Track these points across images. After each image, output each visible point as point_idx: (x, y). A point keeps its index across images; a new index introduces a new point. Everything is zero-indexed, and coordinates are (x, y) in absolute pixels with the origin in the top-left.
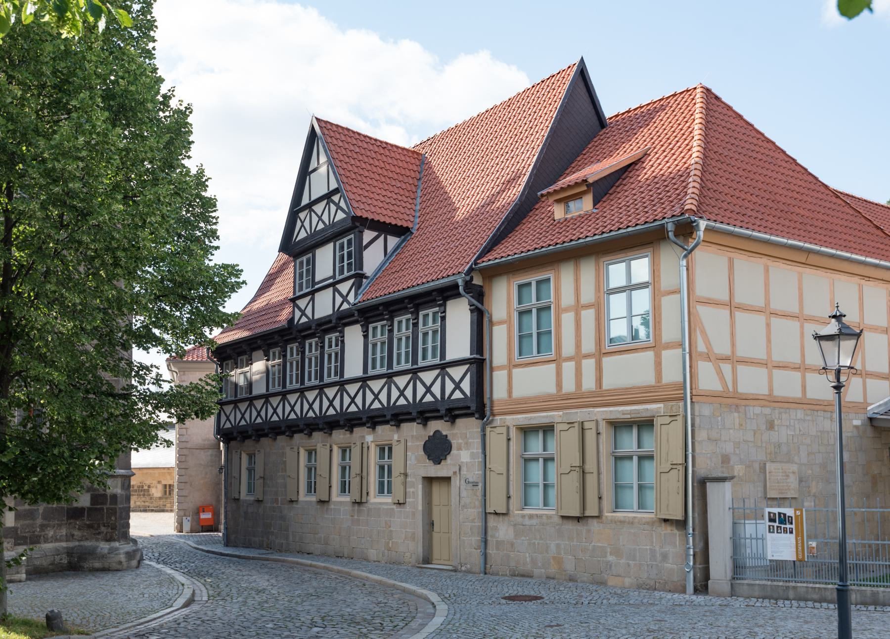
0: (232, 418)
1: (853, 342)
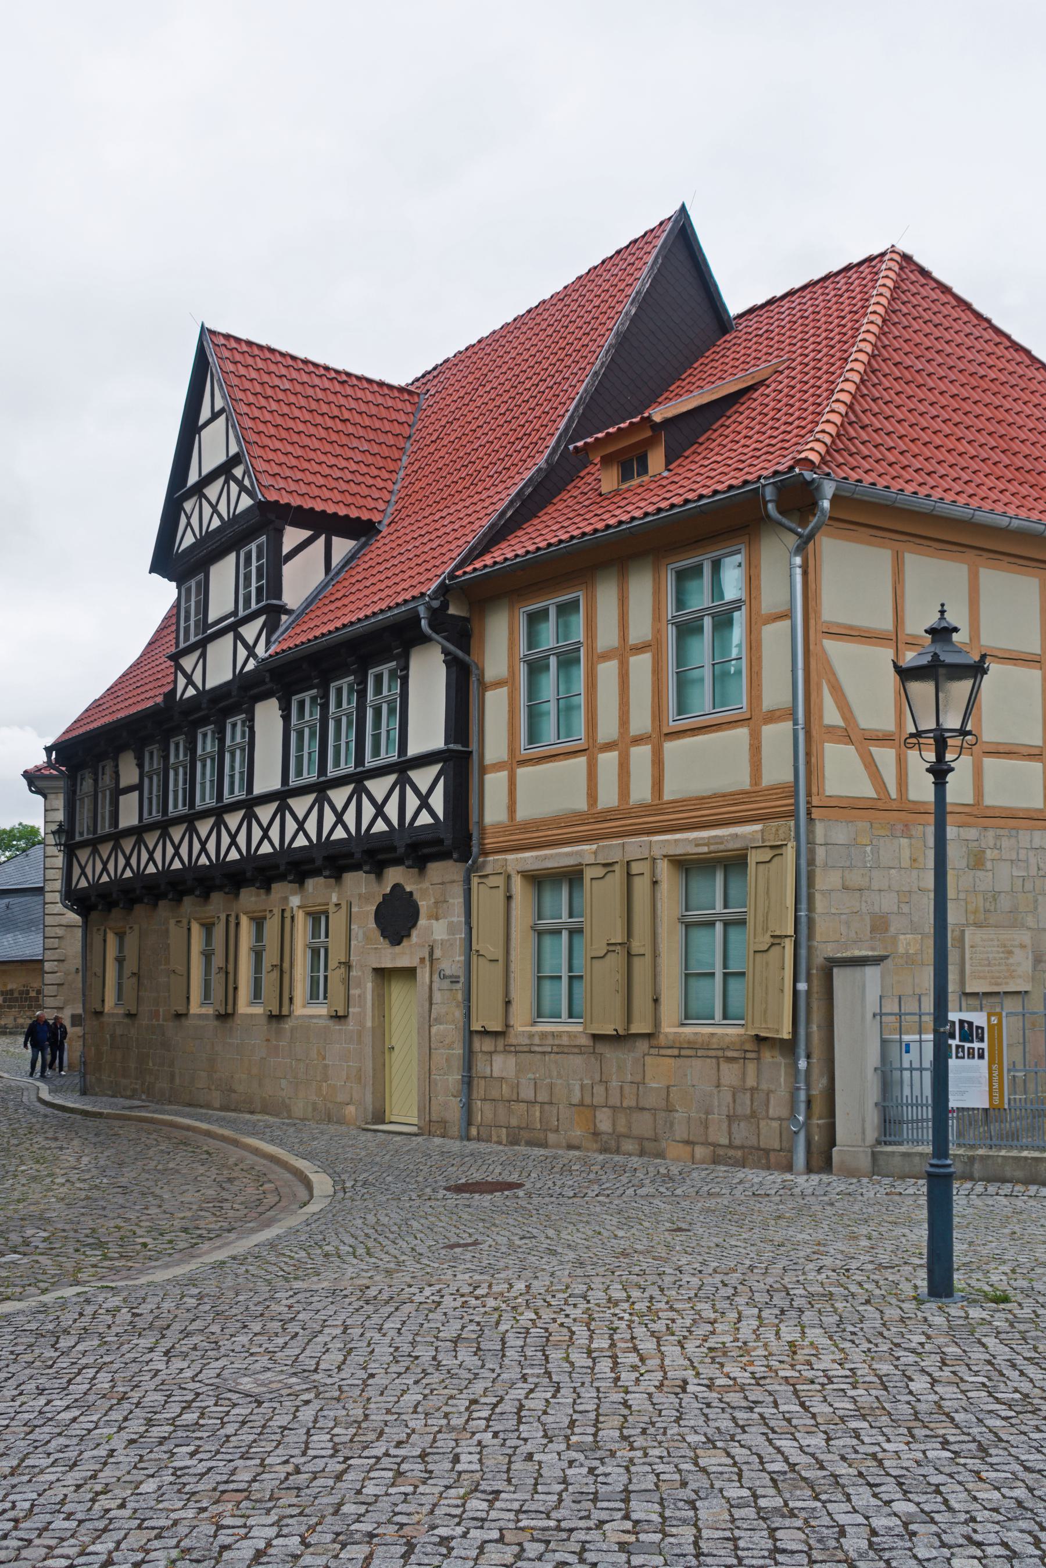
0: (89, 871)
1: (967, 685)
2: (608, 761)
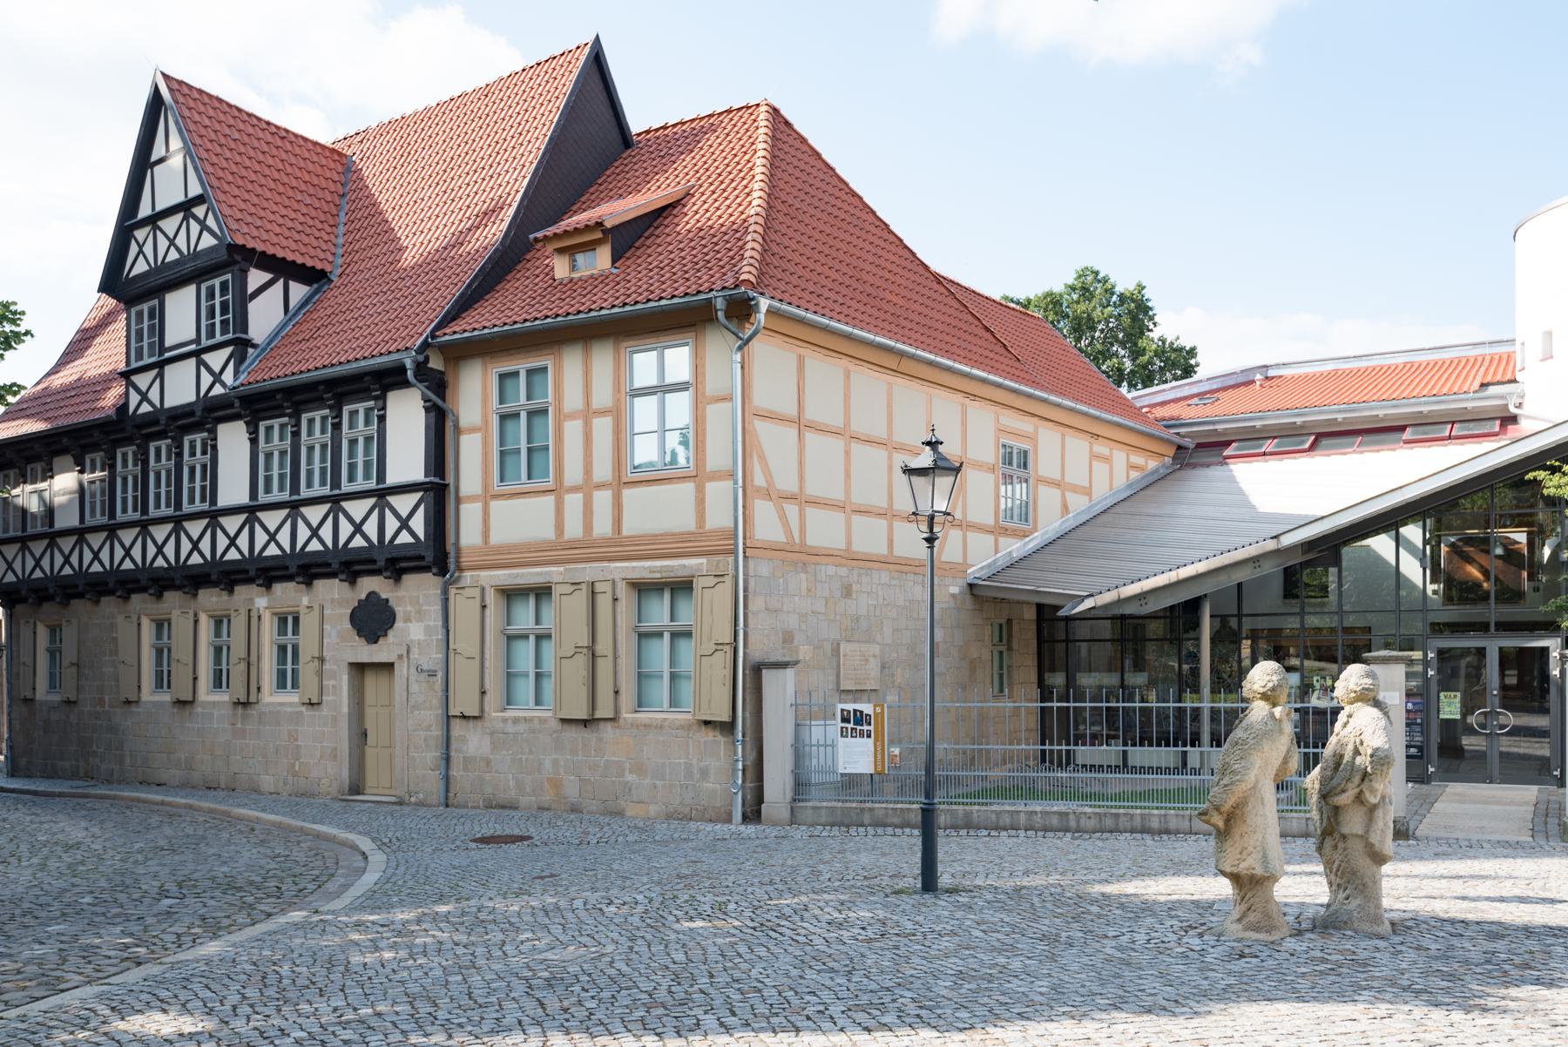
2: (573, 502)
